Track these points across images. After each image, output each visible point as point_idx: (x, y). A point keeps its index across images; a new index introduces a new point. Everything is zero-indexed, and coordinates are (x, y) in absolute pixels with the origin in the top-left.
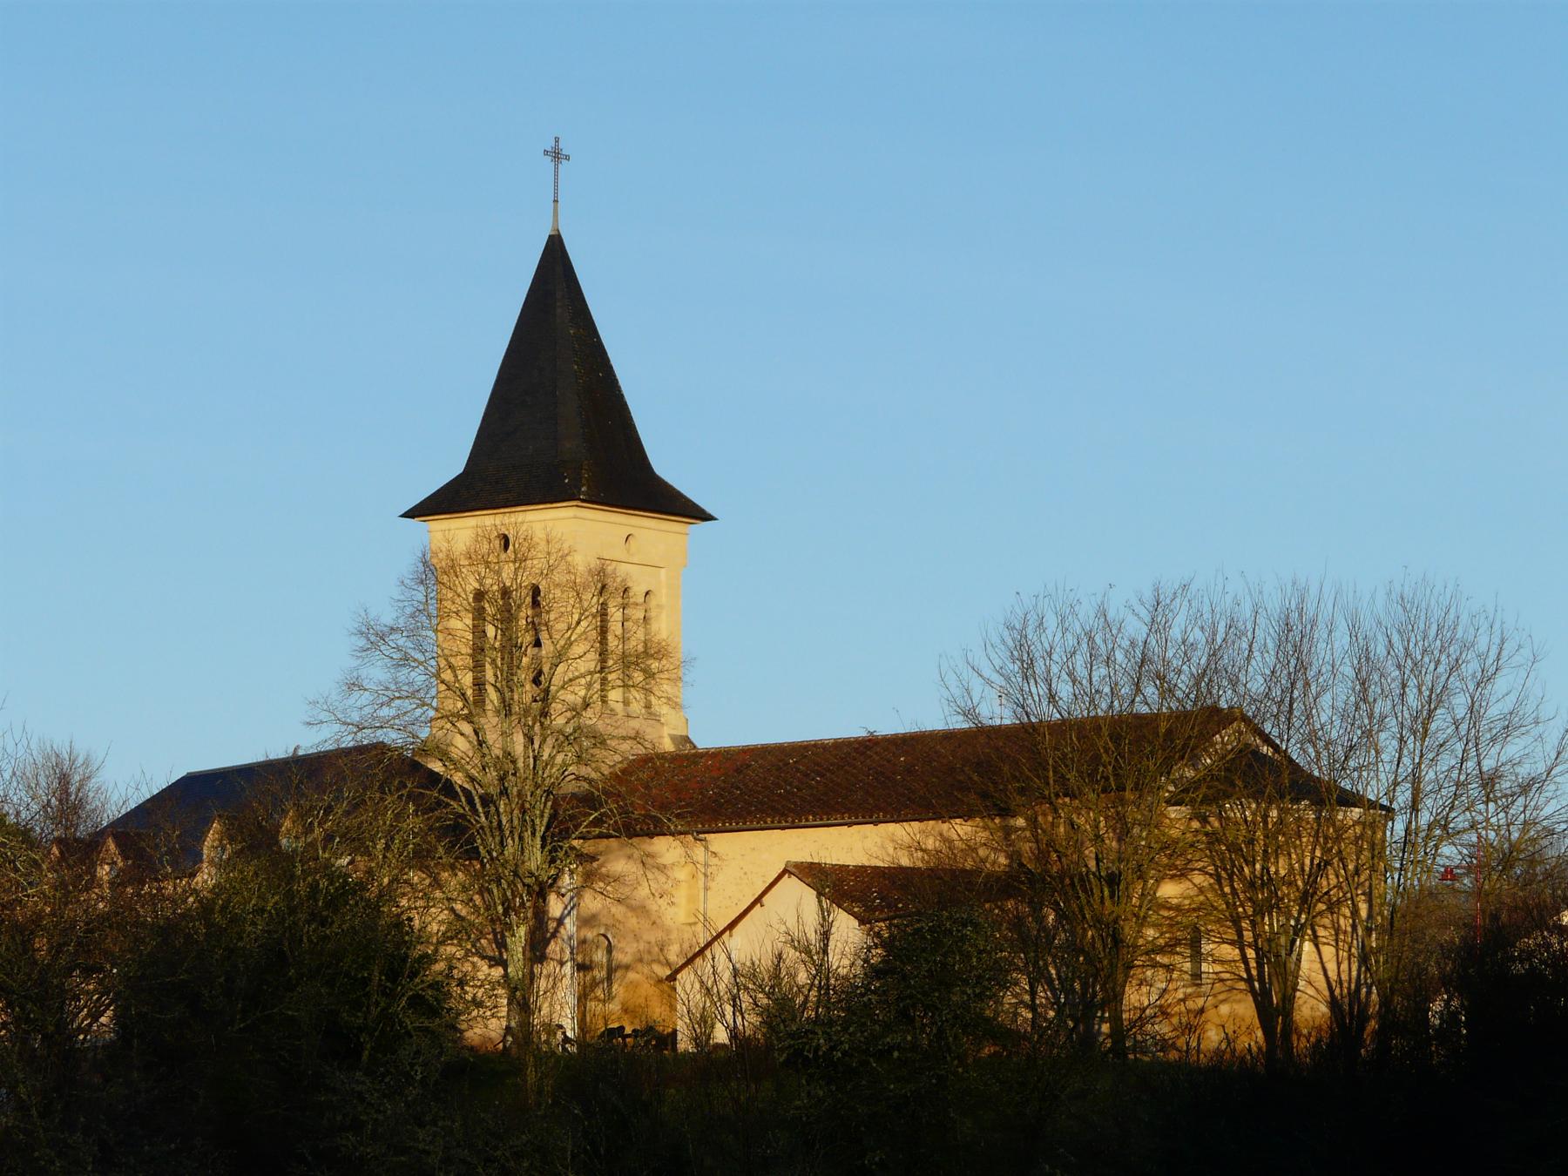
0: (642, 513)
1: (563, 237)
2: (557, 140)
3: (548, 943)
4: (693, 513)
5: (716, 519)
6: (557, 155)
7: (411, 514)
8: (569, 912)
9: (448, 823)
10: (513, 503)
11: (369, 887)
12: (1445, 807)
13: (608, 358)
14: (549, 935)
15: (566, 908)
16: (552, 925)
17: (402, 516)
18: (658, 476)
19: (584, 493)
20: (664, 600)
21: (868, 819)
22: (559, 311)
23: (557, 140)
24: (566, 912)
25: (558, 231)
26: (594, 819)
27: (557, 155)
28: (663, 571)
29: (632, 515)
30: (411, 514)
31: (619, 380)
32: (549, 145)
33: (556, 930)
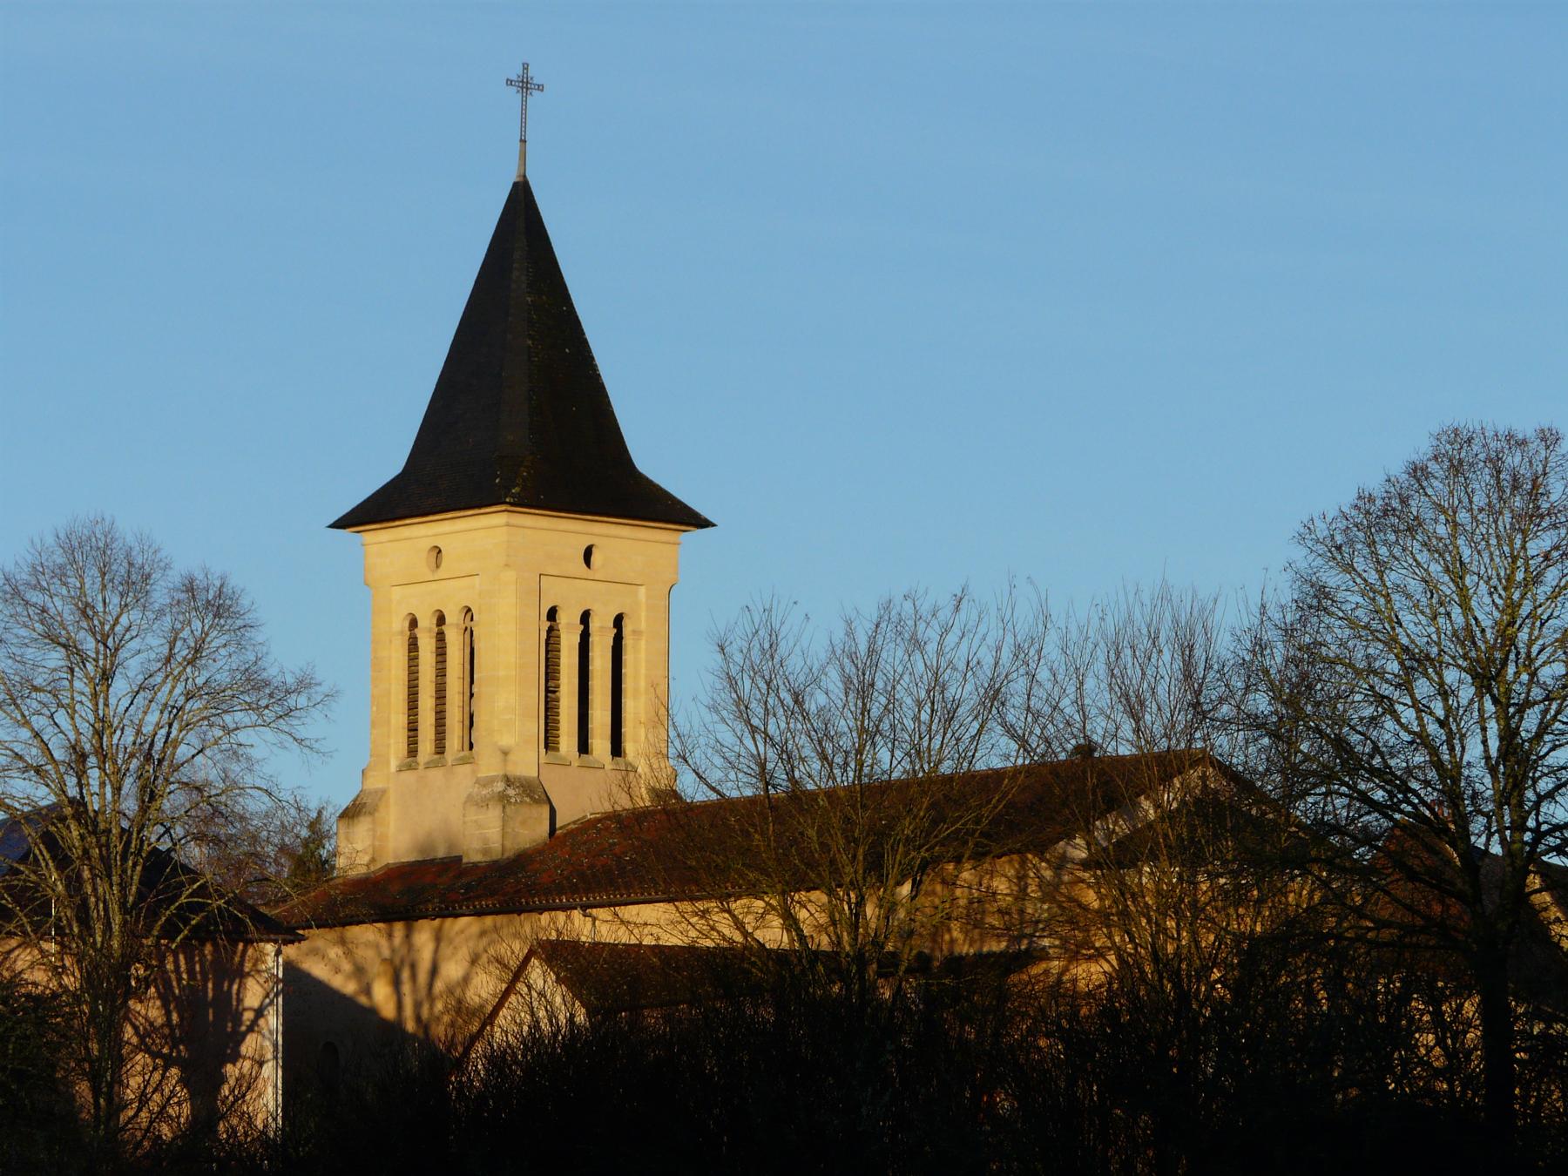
0: (537, 512)
1: (531, 183)
2: (525, 67)
3: (243, 1036)
4: (683, 517)
5: (714, 525)
6: (525, 85)
7: (341, 524)
8: (271, 1003)
9: (1305, 892)
10: (439, 509)
11: (1170, 949)
12: (98, 899)
13: (582, 330)
14: (243, 1028)
15: (267, 996)
16: (248, 1016)
17: (331, 526)
18: (640, 474)
19: (513, 496)
20: (643, 626)
21: (660, 896)
22: (515, 274)
23: (525, 67)
24: (267, 1001)
25: (525, 176)
26: (199, 886)
27: (525, 85)
28: (642, 590)
29: (597, 521)
30: (341, 524)
31: (596, 358)
32: (515, 73)
33: (254, 1022)
